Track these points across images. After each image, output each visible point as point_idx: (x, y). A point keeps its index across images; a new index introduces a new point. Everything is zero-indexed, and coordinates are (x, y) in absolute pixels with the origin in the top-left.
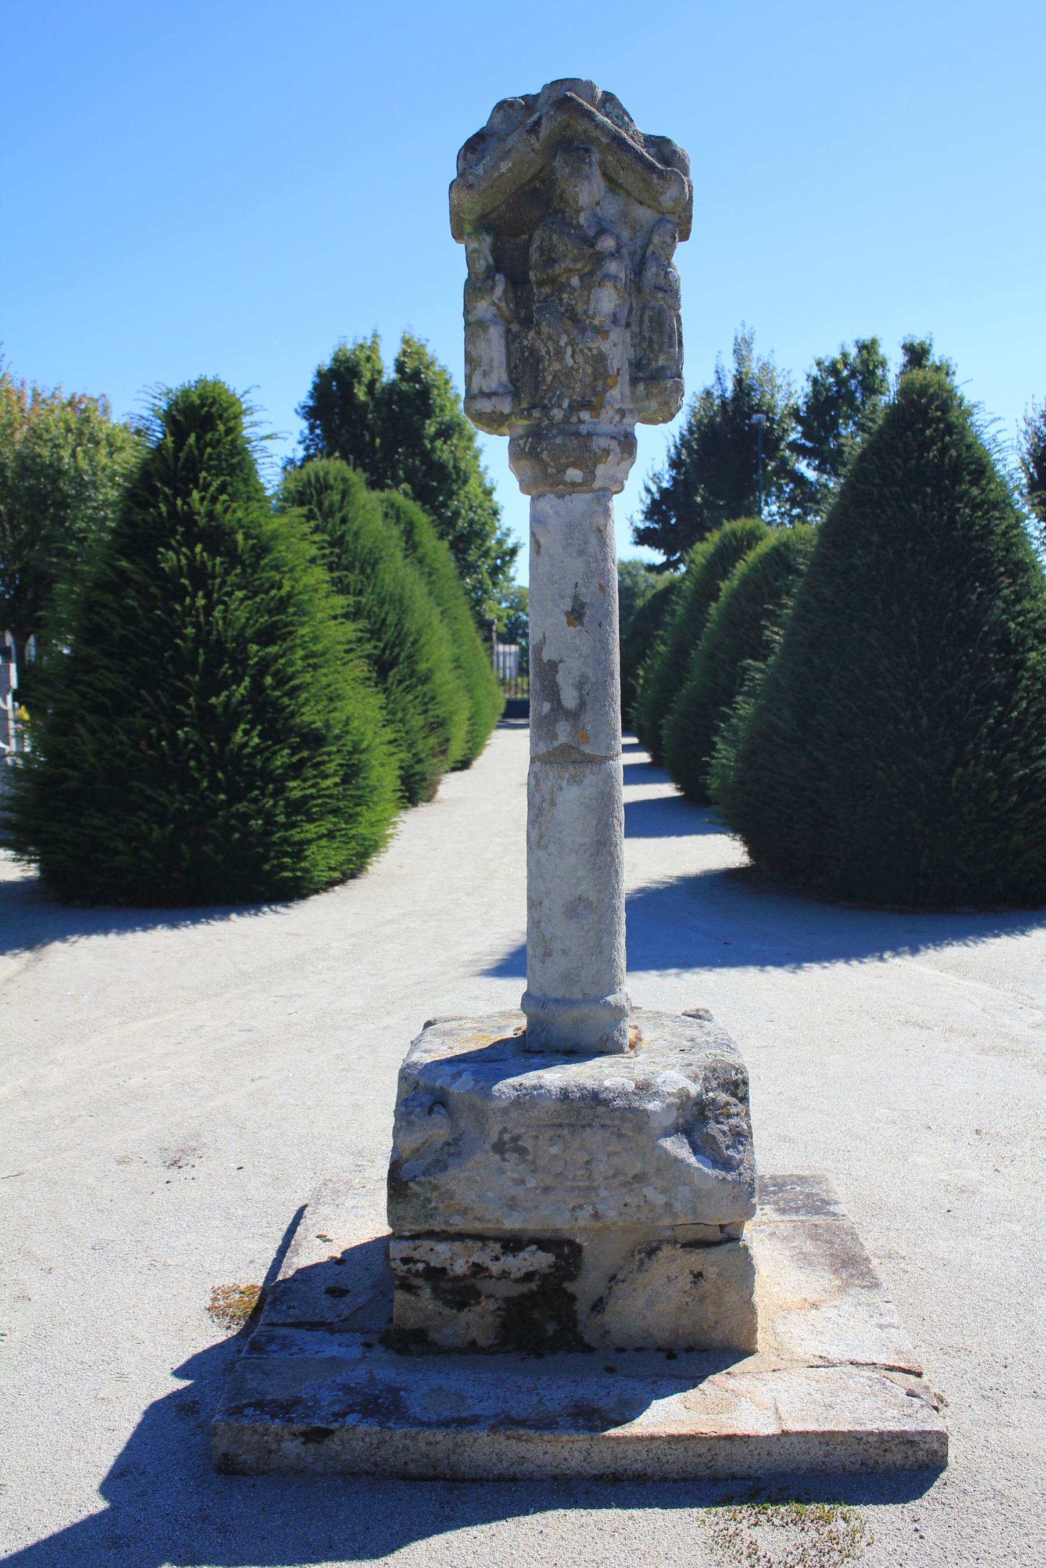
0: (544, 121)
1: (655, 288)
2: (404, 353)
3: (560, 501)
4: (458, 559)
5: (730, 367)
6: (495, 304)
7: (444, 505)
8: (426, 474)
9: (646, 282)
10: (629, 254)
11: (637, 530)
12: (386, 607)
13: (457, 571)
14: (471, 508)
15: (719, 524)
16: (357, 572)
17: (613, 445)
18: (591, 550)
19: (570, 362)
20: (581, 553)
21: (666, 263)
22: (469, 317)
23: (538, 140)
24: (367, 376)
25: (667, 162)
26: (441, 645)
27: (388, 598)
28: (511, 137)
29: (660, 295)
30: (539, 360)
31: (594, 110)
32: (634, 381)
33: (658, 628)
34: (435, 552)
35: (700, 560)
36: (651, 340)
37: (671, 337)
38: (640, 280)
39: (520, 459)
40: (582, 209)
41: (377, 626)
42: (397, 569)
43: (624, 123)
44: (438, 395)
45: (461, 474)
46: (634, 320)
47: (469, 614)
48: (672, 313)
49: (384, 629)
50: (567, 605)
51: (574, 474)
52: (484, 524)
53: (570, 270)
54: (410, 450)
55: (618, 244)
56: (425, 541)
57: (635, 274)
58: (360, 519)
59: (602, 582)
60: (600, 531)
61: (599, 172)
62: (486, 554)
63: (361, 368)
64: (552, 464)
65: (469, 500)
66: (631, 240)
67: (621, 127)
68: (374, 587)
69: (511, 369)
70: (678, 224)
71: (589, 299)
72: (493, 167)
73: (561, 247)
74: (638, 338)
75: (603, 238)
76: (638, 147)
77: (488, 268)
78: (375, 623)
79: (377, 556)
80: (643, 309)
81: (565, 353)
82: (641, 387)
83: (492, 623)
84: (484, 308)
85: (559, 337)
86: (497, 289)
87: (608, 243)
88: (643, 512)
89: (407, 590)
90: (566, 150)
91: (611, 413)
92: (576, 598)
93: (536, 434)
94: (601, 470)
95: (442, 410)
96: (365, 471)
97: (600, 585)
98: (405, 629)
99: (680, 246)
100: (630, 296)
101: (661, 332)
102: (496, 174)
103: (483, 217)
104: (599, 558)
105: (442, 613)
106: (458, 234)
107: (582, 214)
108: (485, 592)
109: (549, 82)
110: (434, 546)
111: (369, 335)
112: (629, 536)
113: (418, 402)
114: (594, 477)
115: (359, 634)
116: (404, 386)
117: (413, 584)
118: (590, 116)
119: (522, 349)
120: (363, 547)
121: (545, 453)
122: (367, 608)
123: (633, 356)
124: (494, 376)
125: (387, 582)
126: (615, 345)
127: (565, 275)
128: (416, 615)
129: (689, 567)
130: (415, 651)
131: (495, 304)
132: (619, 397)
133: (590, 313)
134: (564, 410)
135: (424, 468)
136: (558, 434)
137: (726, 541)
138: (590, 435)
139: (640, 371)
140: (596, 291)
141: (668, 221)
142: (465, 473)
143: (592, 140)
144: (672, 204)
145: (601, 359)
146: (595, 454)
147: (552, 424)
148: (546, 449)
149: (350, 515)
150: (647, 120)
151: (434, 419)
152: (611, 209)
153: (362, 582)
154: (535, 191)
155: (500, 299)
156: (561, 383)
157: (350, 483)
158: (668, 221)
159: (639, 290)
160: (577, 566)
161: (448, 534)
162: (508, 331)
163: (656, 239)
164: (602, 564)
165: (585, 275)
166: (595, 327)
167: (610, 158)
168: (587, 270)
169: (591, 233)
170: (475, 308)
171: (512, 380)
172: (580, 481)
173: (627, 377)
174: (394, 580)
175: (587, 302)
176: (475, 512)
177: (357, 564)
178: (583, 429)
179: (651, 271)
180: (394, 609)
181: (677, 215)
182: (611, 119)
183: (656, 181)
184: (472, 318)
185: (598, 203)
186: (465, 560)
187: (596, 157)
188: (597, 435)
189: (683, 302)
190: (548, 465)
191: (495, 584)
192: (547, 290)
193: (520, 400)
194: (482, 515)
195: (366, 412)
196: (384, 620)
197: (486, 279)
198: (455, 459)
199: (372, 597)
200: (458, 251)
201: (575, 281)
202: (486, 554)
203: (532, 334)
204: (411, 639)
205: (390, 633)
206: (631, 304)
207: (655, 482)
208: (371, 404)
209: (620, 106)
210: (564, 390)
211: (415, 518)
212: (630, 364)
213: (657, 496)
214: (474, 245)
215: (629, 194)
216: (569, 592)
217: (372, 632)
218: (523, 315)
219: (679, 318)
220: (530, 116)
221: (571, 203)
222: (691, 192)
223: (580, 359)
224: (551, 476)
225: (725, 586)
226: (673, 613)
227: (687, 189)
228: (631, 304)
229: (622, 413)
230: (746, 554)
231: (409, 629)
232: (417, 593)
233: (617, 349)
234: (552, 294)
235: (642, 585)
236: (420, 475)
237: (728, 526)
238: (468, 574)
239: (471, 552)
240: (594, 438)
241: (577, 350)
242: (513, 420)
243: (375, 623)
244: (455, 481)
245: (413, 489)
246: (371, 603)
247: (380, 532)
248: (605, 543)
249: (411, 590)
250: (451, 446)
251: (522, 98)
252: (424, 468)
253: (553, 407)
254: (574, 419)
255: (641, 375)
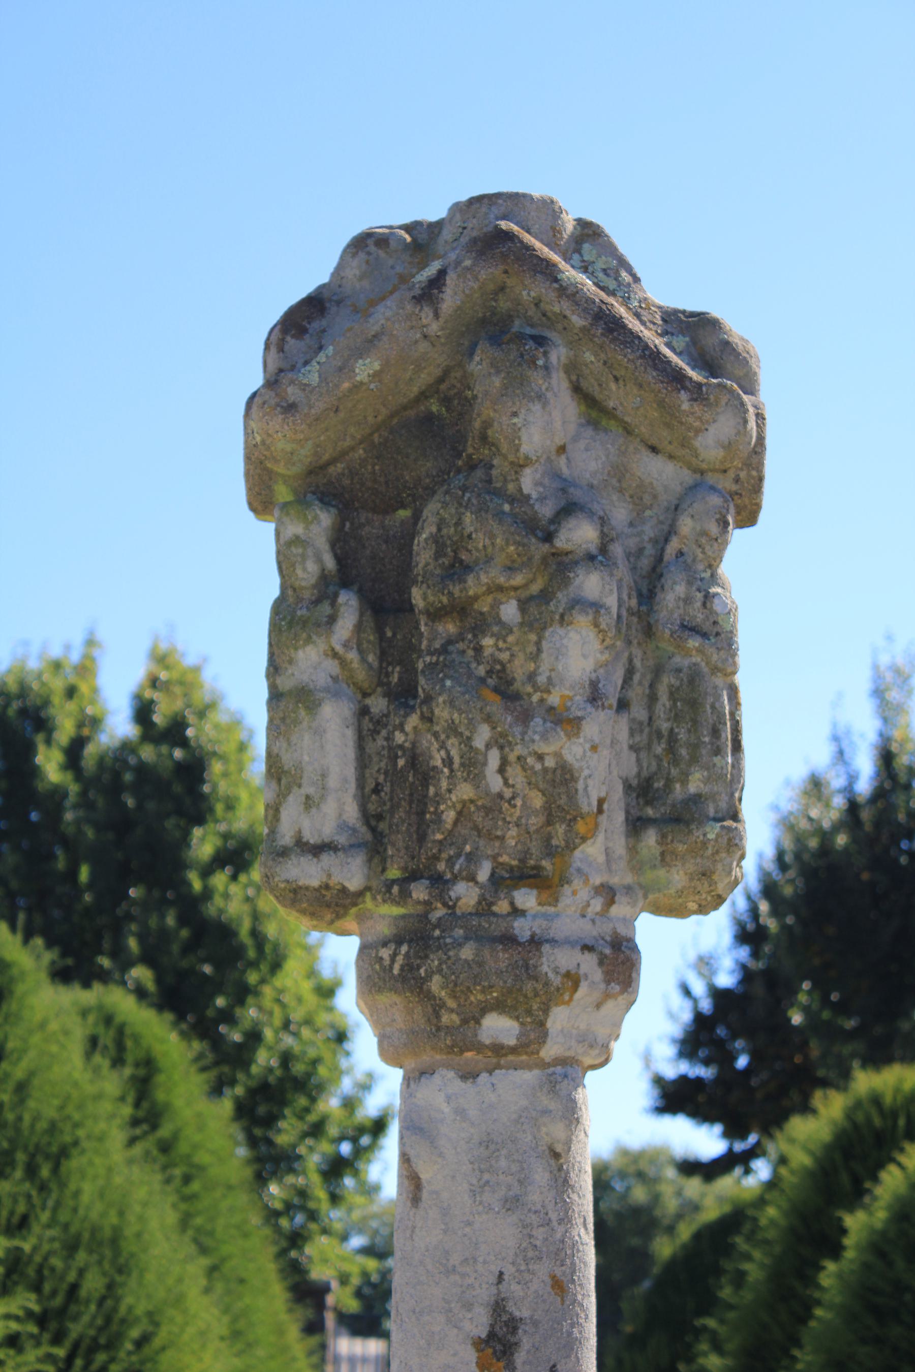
0: (451, 279)
1: (683, 627)
2: (153, 682)
3: (467, 1086)
4: (253, 1142)
5: (865, 729)
6: (335, 655)
7: (227, 1017)
8: (189, 948)
9: (663, 614)
10: (628, 555)
11: (658, 1081)
12: (81, 1257)
13: (248, 1172)
14: (286, 1024)
15: (841, 1079)
16: (19, 1174)
17: (588, 964)
18: (535, 1197)
19: (495, 783)
20: (512, 1203)
21: (707, 575)
22: (279, 681)
23: (437, 315)
24: (65, 730)
25: (711, 367)
26: (203, 1346)
27: (86, 1235)
28: (380, 308)
29: (694, 643)
30: (427, 776)
31: (555, 258)
32: (636, 825)
33: (704, 1311)
34: (201, 1128)
35: (801, 1159)
36: (672, 738)
37: (716, 732)
38: (651, 611)
39: (380, 990)
40: (527, 462)
41: (58, 1301)
42: (110, 1170)
43: (620, 284)
44: (226, 775)
45: (268, 949)
46: (637, 693)
47: (271, 1268)
48: (719, 681)
49: (73, 1308)
50: (479, 1323)
51: (499, 1027)
52: (315, 1062)
53: (500, 589)
54: (156, 893)
55: (603, 535)
56: (178, 1103)
57: (640, 595)
58: (32, 1054)
59: (558, 1272)
60: (556, 1155)
61: (565, 384)
62: (317, 1130)
63: (52, 711)
64: (452, 1004)
65: (283, 1006)
66: (631, 524)
67: (612, 293)
68: (55, 1210)
69: (367, 792)
70: (733, 494)
71: (539, 650)
72: (340, 369)
73: (481, 540)
74: (645, 736)
75: (572, 522)
76: (650, 336)
77: (324, 577)
78: (54, 1293)
79: (68, 1139)
80: (658, 671)
81: (485, 764)
82: (651, 838)
83: (325, 1289)
84: (311, 662)
85: (472, 725)
86: (340, 623)
87: (581, 534)
88: (674, 1041)
89: (132, 1218)
90: (495, 340)
91: (584, 894)
92: (498, 1307)
93: (417, 937)
94: (559, 1019)
95: (230, 806)
96: (49, 945)
97: (553, 1277)
98: (123, 1310)
99: (739, 538)
100: (629, 643)
101: (695, 722)
102: (346, 385)
103: (315, 470)
104: (553, 1216)
105: (212, 1270)
106: (261, 502)
107: (528, 471)
108: (313, 1216)
109: (464, 197)
110: (199, 1115)
111: (78, 640)
112: (642, 1094)
113: (177, 788)
114: (543, 1036)
115: (14, 1326)
116: (148, 753)
117: (145, 1204)
118: (548, 270)
119: (393, 752)
120: (36, 1119)
121: (436, 978)
122: (38, 1259)
123: (635, 770)
124: (330, 808)
125: (85, 1198)
126: (594, 748)
127: (489, 599)
128: (150, 1277)
129: (775, 1173)
130: (143, 1362)
131: (335, 655)
132: (601, 859)
133: (541, 679)
134: (482, 887)
135: (185, 933)
136: (467, 938)
137: (860, 1117)
138: (536, 942)
139: (648, 803)
140: (555, 635)
141: (713, 488)
142: (276, 947)
143: (549, 319)
144: (721, 453)
145: (562, 778)
146: (547, 984)
147: (454, 916)
148: (440, 971)
149: (10, 1045)
150: (668, 277)
151: (211, 826)
152: (589, 461)
153: (29, 1197)
154: (429, 418)
155: (346, 645)
156: (476, 828)
157: (15, 971)
158: (713, 488)
159: (649, 631)
160: (501, 1235)
161: (233, 1082)
162: (364, 712)
163: (686, 525)
164: (560, 1230)
165: (531, 598)
166: (551, 709)
167: (589, 357)
168: (535, 588)
169: (546, 511)
170: (291, 662)
171: (371, 819)
172: (512, 1042)
173: (620, 817)
174: (101, 1195)
175: (535, 656)
176: (296, 1035)
177: (21, 1157)
178: (522, 928)
179: (674, 593)
180: (100, 1263)
181: (731, 474)
182: (592, 275)
183: (685, 406)
184: (285, 683)
185: (562, 449)
186: (270, 1142)
187: (559, 354)
188: (553, 942)
189: (743, 658)
190: (443, 1005)
191: (335, 1199)
192: (450, 628)
193: (384, 861)
194: (312, 1043)
195: (59, 809)
196: (74, 1289)
197: (317, 602)
198: (256, 916)
199: (50, 1233)
200: (261, 538)
201: (510, 611)
202: (317, 1130)
203: (413, 721)
204: (135, 1333)
205: (86, 1319)
206: (630, 661)
207: (700, 974)
208: (74, 788)
209: (610, 249)
210: (482, 843)
211: (158, 1049)
212: (628, 787)
213: (706, 1005)
214: (295, 529)
215: (628, 431)
216: (484, 1293)
217: (42, 1320)
218: (395, 678)
219: (733, 691)
220: (423, 265)
221: (504, 447)
222: (761, 427)
223: (516, 775)
224: (449, 1030)
225: (858, 1224)
226: (739, 1279)
227: (752, 424)
228: (630, 661)
229: (609, 894)
230: (902, 1150)
231: (130, 1309)
232: (154, 1224)
233: (599, 758)
234: (461, 637)
235: (671, 1204)
236: (175, 948)
237: (865, 1081)
238: (275, 1174)
239: (282, 1124)
240: (546, 948)
241: (512, 757)
242: (368, 902)
243: (54, 1293)
244: (253, 965)
245: (159, 980)
246: (46, 1247)
247: (76, 1084)
248: (566, 1181)
249: (141, 1219)
250: (246, 886)
251: (408, 228)
252: (185, 933)
253: (455, 878)
254: (502, 907)
255: (650, 812)
